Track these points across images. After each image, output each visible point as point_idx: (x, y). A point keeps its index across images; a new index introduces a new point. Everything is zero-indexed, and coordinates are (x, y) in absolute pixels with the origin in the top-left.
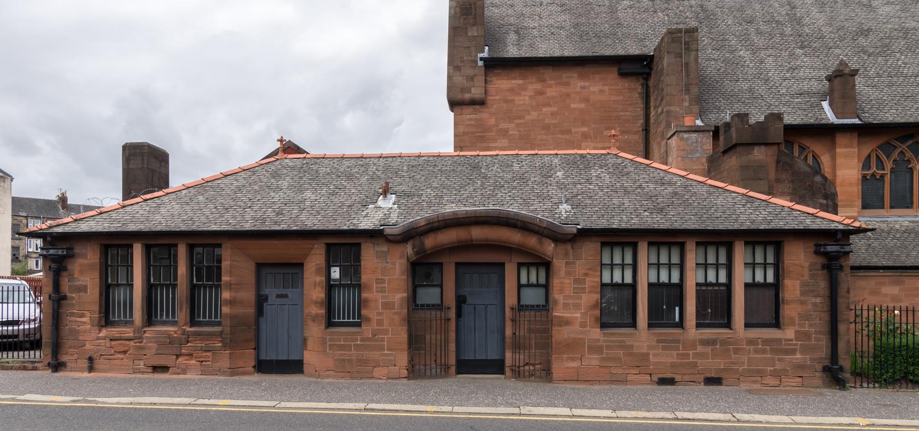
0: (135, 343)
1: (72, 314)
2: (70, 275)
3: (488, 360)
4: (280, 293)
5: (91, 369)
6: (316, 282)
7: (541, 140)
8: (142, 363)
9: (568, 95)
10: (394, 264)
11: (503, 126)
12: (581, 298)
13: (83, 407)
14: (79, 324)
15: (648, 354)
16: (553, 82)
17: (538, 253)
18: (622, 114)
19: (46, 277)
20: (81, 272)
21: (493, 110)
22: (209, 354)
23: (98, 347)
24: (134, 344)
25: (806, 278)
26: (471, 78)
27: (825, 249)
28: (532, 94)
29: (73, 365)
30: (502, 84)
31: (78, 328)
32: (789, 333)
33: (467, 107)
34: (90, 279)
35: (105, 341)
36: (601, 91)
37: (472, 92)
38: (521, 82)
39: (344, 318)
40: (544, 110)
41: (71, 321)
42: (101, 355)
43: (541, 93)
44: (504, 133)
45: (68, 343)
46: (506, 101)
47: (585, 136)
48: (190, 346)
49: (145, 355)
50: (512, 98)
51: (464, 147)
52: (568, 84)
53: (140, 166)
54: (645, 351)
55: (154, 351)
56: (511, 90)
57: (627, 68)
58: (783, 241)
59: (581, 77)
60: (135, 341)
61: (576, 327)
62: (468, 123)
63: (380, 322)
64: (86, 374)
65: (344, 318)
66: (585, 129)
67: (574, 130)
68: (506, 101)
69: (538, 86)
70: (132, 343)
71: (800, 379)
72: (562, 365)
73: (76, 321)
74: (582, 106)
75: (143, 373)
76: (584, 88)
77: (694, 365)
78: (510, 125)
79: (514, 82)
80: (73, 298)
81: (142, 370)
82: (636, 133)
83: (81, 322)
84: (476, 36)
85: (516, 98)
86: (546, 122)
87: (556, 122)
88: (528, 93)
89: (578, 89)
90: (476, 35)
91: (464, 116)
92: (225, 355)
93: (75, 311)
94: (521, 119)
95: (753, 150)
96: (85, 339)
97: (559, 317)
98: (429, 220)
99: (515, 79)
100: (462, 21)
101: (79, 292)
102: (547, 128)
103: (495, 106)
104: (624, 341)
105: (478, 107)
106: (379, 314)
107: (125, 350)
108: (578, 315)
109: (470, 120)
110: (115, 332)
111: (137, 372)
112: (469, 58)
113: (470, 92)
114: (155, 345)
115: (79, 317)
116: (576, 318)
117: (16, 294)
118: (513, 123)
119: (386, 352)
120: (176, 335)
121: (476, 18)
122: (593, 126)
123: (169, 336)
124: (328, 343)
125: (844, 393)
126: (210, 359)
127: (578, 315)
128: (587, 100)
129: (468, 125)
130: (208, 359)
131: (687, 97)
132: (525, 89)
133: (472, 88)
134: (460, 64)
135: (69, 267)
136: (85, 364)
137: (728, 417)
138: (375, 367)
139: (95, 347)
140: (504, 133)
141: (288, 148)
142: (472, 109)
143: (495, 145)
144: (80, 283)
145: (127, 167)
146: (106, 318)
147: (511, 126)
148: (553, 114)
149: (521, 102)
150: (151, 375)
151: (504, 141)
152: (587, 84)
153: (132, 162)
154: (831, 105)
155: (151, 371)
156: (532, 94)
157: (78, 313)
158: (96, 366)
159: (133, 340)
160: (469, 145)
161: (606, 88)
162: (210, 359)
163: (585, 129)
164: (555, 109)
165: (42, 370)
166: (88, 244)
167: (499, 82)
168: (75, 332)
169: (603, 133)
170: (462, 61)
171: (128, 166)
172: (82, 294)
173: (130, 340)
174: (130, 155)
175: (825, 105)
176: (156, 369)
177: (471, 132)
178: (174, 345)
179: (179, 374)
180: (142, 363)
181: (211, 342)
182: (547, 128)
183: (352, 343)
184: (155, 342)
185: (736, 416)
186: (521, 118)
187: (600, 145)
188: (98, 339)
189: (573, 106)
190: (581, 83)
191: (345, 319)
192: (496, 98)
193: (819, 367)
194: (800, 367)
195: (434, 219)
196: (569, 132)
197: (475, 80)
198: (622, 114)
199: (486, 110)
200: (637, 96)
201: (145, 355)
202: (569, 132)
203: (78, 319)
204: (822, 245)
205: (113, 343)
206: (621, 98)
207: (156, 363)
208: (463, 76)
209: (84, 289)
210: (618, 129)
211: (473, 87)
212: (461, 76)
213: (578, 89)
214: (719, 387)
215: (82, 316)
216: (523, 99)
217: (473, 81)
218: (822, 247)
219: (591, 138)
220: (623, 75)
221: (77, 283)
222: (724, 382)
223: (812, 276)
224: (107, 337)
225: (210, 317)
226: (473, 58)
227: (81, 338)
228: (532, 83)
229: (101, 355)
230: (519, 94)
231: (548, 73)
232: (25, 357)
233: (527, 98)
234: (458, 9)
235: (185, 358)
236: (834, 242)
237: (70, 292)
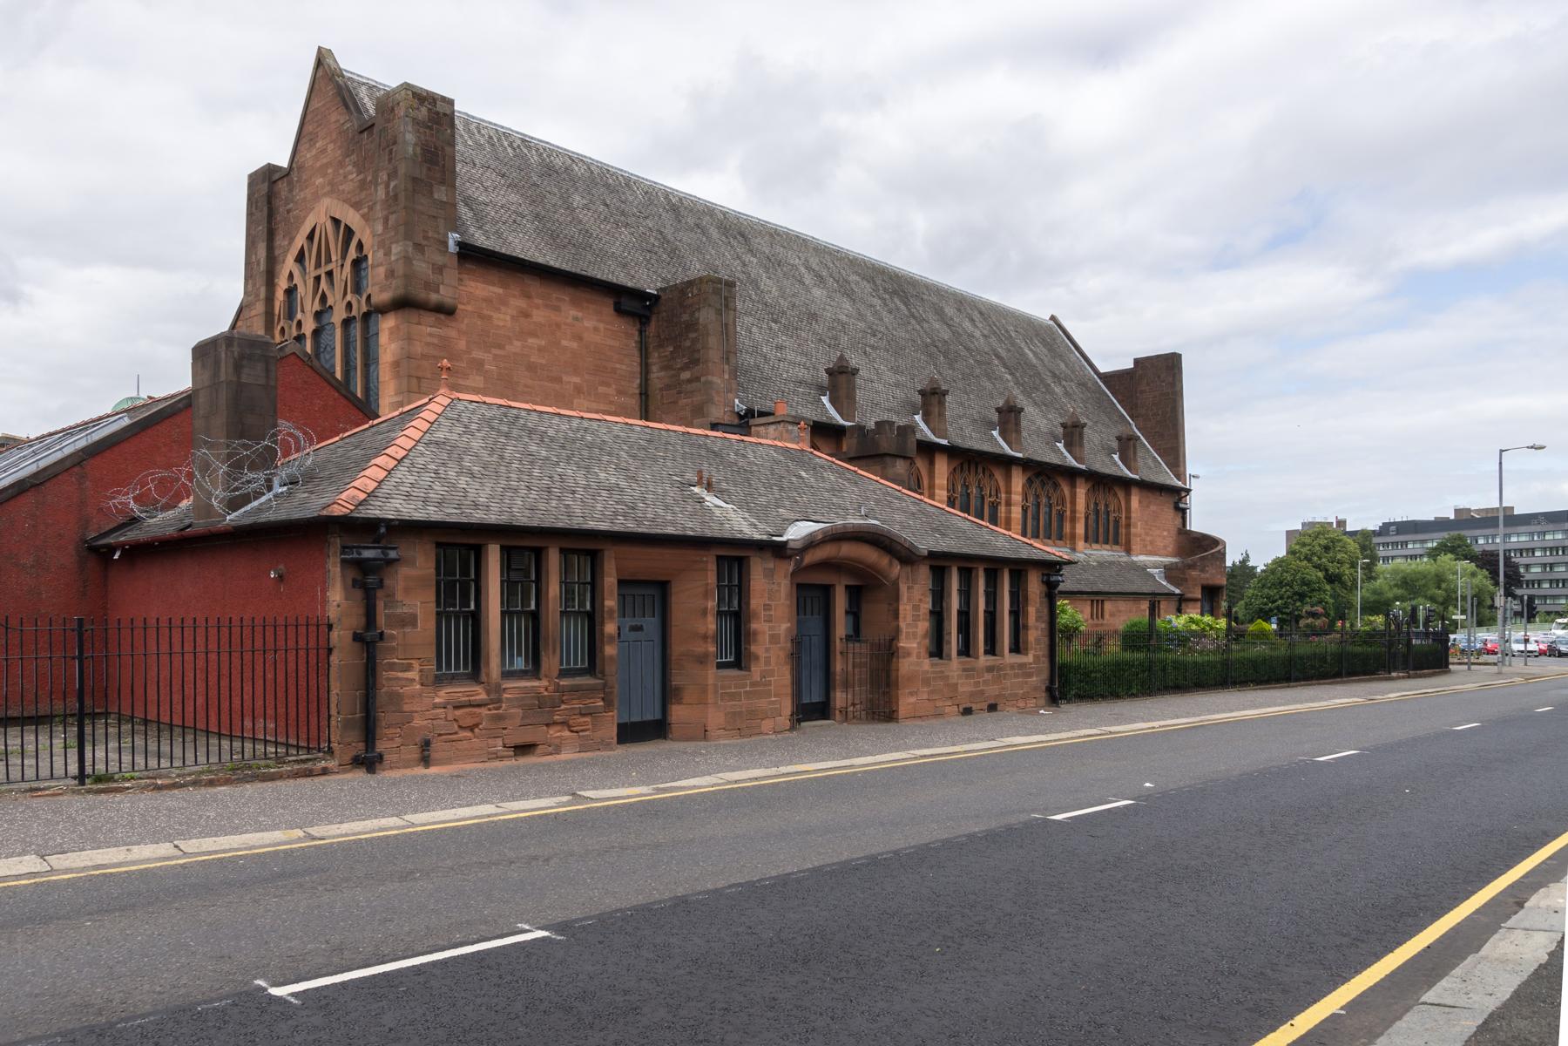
0: (490, 710)
1: (392, 667)
2: (388, 596)
3: (812, 703)
4: (634, 624)
5: (426, 761)
6: (706, 609)
7: (526, 386)
8: (499, 742)
9: (558, 326)
10: (779, 584)
11: (477, 354)
12: (916, 627)
13: (983, 755)
14: (404, 682)
15: (957, 684)
16: (540, 302)
17: (882, 575)
18: (618, 366)
19: (346, 599)
20: (407, 590)
21: (463, 327)
22: (588, 719)
23: (435, 722)
24: (489, 712)
25: (1038, 605)
26: (439, 269)
27: (360, 554)
28: (515, 313)
29: (394, 757)
30: (477, 290)
31: (401, 691)
32: (1029, 658)
33: (429, 314)
34: (422, 603)
35: (444, 710)
36: (596, 329)
37: (441, 292)
38: (500, 291)
39: (726, 658)
40: (530, 340)
41: (390, 679)
42: (440, 735)
43: (527, 315)
44: (478, 365)
45: (385, 718)
46: (481, 317)
47: (578, 390)
48: (566, 709)
49: (504, 729)
50: (488, 313)
51: (424, 378)
52: (557, 309)
53: (262, 381)
54: (955, 681)
55: (518, 721)
56: (488, 300)
57: (627, 304)
58: (547, 548)
59: (575, 303)
60: (491, 706)
61: (913, 658)
62: (429, 339)
63: (767, 662)
64: (420, 771)
65: (726, 658)
66: (577, 380)
67: (565, 378)
68: (481, 317)
69: (521, 303)
70: (484, 711)
71: (1035, 700)
72: (906, 702)
73: (398, 679)
74: (575, 345)
75: (501, 758)
76: (576, 319)
77: (982, 692)
78: (486, 355)
79: (491, 288)
80: (393, 637)
81: (499, 754)
82: (632, 395)
83: (407, 679)
84: (445, 203)
85: (495, 315)
86: (532, 360)
87: (544, 362)
88: (509, 311)
89: (570, 320)
90: (445, 200)
91: (424, 328)
92: (608, 719)
93: (396, 660)
94: (500, 349)
95: (896, 462)
96: (414, 709)
97: (902, 647)
98: (825, 533)
99: (494, 285)
100: (424, 171)
101: (403, 626)
102: (532, 368)
103: (466, 322)
104: (943, 672)
105: (442, 317)
106: (767, 650)
107: (475, 723)
108: (915, 645)
109: (430, 335)
110: (459, 695)
111: (494, 758)
112: (436, 236)
113: (437, 291)
114: (519, 711)
115: (401, 671)
116: (914, 648)
117: (201, 632)
118: (490, 353)
119: (773, 699)
120: (546, 693)
121: (444, 172)
122: (586, 377)
123: (539, 697)
124: (720, 691)
125: (374, 776)
126: (590, 727)
127: (915, 645)
128: (579, 338)
129: (428, 344)
130: (587, 727)
131: (726, 367)
132: (504, 303)
133: (441, 286)
134: (424, 243)
135: (387, 582)
136: (413, 752)
137: (299, 833)
138: (763, 719)
139: (430, 721)
140: (478, 365)
141: (291, 354)
142: (433, 319)
143: (467, 383)
144: (405, 610)
145: (234, 379)
146: (937, 649)
147: (487, 357)
148: (540, 349)
149: (501, 324)
150: (512, 762)
151: (478, 378)
152: (580, 315)
153: (246, 370)
154: (832, 401)
155: (512, 753)
156: (515, 313)
157: (403, 664)
158: (434, 755)
159: (485, 705)
160: (429, 376)
161: (601, 326)
162: (590, 727)
163: (577, 380)
164: (543, 343)
165: (338, 773)
166: (417, 541)
167: (472, 284)
168: (396, 699)
169: (597, 388)
170: (426, 238)
171: (239, 377)
172: (408, 630)
173: (479, 706)
174: (242, 357)
175: (825, 400)
176: (524, 749)
177: (434, 356)
178: (541, 709)
179: (551, 754)
180: (499, 742)
181: (592, 701)
182: (532, 368)
183: (742, 690)
184: (519, 707)
185: (182, 847)
186: (501, 347)
187: (594, 406)
188: (436, 706)
189: (564, 343)
190: (573, 312)
191: (460, 669)
192: (469, 308)
193: (1044, 688)
194: (1036, 689)
195: (828, 531)
196: (558, 380)
197: (444, 274)
198: (618, 366)
199: (454, 324)
200: (634, 345)
201: (504, 729)
202: (558, 380)
203: (400, 675)
204: (354, 547)
205: (458, 712)
206: (617, 344)
207: (519, 741)
208: (428, 263)
209: (411, 620)
210: (614, 386)
211: (442, 283)
212: (424, 261)
213: (570, 320)
214: (969, 717)
215: (409, 668)
216: (503, 319)
217: (442, 274)
218: (355, 550)
219: (583, 393)
220: (619, 311)
221: (399, 611)
222: (999, 708)
223: (1041, 603)
224: (448, 703)
225: (457, 667)
226: (441, 237)
227: (406, 708)
228: (514, 296)
229: (440, 735)
230: (498, 310)
231: (535, 286)
232: (187, 763)
233: (508, 318)
234: (418, 150)
235: (559, 728)
236: (372, 543)
237: (390, 626)
